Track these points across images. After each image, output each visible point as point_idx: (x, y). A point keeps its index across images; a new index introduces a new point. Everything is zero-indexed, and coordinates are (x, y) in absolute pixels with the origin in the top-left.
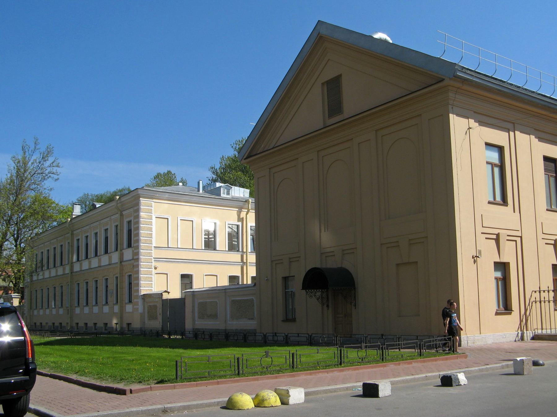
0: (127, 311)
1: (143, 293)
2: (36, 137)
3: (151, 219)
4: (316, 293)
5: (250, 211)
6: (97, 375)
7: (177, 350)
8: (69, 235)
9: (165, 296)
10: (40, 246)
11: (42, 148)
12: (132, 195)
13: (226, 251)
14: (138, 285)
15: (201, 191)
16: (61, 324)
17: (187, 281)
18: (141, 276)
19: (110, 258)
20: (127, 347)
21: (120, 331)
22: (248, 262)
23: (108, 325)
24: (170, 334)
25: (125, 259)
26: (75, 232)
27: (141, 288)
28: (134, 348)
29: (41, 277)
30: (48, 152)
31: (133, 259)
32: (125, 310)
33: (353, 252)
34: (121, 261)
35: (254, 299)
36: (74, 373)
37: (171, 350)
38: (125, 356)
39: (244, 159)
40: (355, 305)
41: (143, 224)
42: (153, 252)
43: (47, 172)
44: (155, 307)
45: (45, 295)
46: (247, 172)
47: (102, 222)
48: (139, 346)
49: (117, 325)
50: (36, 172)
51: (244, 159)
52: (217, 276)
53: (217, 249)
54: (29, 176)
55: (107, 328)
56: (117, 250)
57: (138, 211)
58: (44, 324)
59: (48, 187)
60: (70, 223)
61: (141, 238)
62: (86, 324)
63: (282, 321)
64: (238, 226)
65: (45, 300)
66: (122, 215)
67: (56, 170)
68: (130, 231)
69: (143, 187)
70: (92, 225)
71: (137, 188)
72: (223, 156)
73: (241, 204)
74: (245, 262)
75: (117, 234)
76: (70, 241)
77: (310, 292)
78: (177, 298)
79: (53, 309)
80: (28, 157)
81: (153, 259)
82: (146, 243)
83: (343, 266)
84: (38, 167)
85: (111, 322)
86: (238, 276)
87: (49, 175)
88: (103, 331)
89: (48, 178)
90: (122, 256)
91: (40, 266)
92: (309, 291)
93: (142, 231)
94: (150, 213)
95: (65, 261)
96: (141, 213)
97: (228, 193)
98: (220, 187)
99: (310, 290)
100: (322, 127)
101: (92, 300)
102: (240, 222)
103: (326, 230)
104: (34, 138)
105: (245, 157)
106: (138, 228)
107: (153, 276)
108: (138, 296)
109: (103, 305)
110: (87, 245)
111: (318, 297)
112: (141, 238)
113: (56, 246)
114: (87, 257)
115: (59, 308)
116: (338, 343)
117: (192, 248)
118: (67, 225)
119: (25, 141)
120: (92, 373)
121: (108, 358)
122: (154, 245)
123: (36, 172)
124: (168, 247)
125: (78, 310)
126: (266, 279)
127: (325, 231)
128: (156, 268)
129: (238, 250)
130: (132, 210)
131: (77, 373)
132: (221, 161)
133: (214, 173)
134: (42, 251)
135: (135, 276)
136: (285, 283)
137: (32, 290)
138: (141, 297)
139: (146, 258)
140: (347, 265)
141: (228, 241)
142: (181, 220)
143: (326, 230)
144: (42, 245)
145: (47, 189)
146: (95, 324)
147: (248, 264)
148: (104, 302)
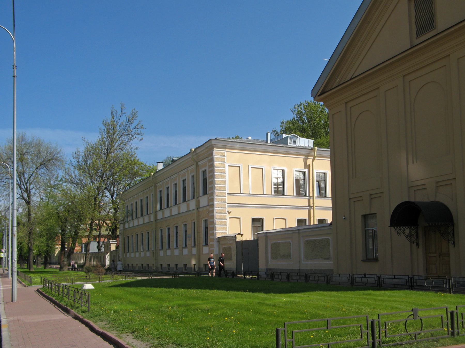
0: (160, 255)
1: (218, 236)
2: (122, 103)
3: (225, 168)
4: (405, 231)
5: (316, 158)
6: (157, 338)
7: (257, 294)
8: (153, 188)
9: (239, 238)
10: (130, 199)
11: (128, 112)
12: (206, 147)
13: (294, 196)
14: (213, 228)
15: (269, 142)
16: (148, 265)
17: (258, 224)
18: (216, 220)
19: (188, 206)
20: (203, 290)
21: (198, 270)
22: (315, 205)
23: (188, 266)
24: (245, 274)
25: (201, 206)
26: (157, 185)
27: (216, 232)
28: (209, 291)
29: (131, 225)
30: (133, 115)
31: (208, 205)
32: (202, 251)
33: (451, 184)
34: (198, 207)
35: (330, 239)
36: (131, 332)
37: (251, 294)
38: (199, 304)
39: (318, 96)
40: (454, 243)
41: (217, 172)
42: (226, 198)
43: (133, 133)
44: (230, 248)
45: (135, 241)
46: (305, 132)
47: (180, 173)
48: (215, 289)
49: (196, 266)
50: (123, 133)
51: (318, 96)
52: (286, 219)
53: (286, 195)
54: (118, 137)
55: (186, 269)
56: (194, 198)
57: (212, 160)
58: (135, 265)
59: (134, 146)
60: (153, 177)
61: (216, 185)
62: (169, 265)
63: (362, 261)
64: (304, 173)
65: (135, 245)
66: (197, 166)
67: (140, 131)
68: (205, 180)
69: (216, 138)
70: (172, 177)
71: (211, 139)
72: (283, 120)
73: (306, 152)
74: (312, 206)
75: (194, 183)
76: (153, 193)
77: (398, 229)
78: (247, 240)
79: (142, 253)
80: (116, 121)
81: (227, 204)
82: (220, 190)
83: (438, 200)
84: (125, 130)
85: (190, 262)
86: (305, 220)
87: (134, 136)
88: (184, 271)
89: (134, 138)
90: (198, 203)
91: (129, 215)
92: (406, 227)
93: (216, 178)
94: (223, 162)
95: (150, 211)
96: (215, 162)
97: (295, 143)
98: (287, 138)
99: (399, 227)
100: (410, 48)
101: (173, 244)
102: (307, 169)
103: (415, 162)
104: (121, 104)
105: (318, 94)
106: (212, 177)
107: (227, 220)
108: (213, 239)
109: (183, 248)
110: (168, 195)
111: (407, 234)
112: (216, 185)
113: (142, 198)
114: (168, 206)
115: (136, 252)
116: (451, 288)
117: (262, 194)
118: (151, 179)
119: (113, 107)
120: (152, 334)
121: (180, 305)
122: (227, 192)
123: (123, 133)
124: (240, 193)
125: (161, 253)
126: (344, 218)
127: (413, 163)
128: (229, 213)
129: (305, 195)
130: (206, 160)
131: (134, 332)
132: (281, 125)
133: (276, 135)
134: (131, 203)
135: (211, 220)
136: (365, 221)
137: (124, 237)
138: (216, 240)
139: (220, 204)
140: (442, 198)
141: (296, 186)
142: (252, 168)
143: (415, 162)
144: (132, 198)
145: (134, 148)
146: (176, 265)
147: (315, 208)
148: (184, 246)
